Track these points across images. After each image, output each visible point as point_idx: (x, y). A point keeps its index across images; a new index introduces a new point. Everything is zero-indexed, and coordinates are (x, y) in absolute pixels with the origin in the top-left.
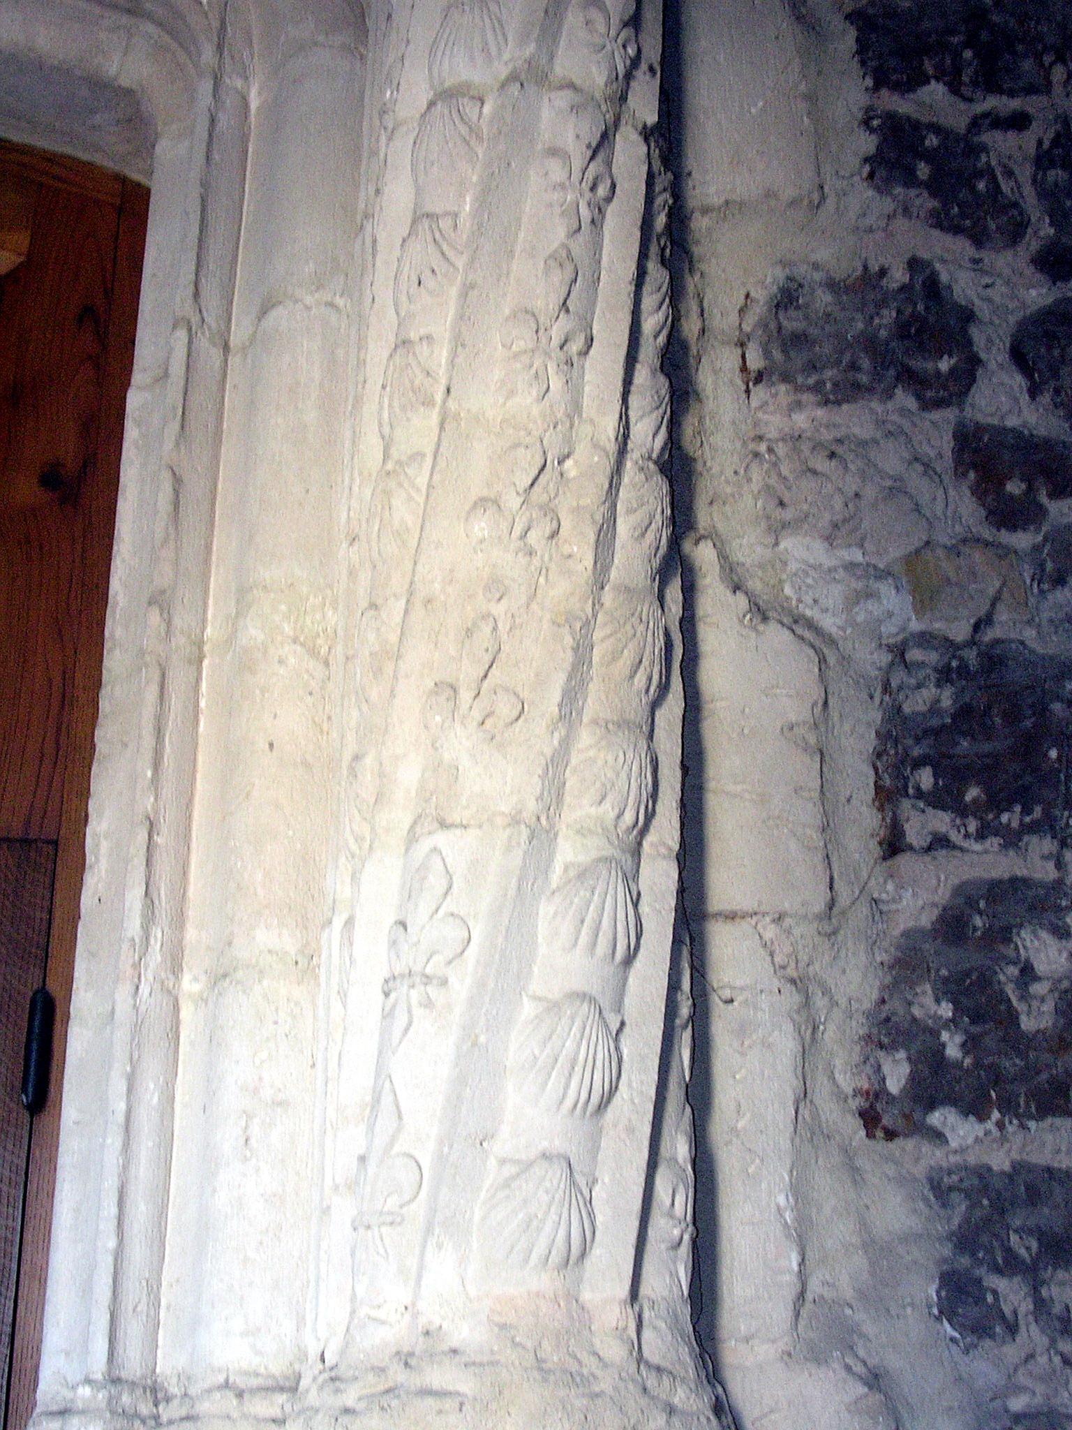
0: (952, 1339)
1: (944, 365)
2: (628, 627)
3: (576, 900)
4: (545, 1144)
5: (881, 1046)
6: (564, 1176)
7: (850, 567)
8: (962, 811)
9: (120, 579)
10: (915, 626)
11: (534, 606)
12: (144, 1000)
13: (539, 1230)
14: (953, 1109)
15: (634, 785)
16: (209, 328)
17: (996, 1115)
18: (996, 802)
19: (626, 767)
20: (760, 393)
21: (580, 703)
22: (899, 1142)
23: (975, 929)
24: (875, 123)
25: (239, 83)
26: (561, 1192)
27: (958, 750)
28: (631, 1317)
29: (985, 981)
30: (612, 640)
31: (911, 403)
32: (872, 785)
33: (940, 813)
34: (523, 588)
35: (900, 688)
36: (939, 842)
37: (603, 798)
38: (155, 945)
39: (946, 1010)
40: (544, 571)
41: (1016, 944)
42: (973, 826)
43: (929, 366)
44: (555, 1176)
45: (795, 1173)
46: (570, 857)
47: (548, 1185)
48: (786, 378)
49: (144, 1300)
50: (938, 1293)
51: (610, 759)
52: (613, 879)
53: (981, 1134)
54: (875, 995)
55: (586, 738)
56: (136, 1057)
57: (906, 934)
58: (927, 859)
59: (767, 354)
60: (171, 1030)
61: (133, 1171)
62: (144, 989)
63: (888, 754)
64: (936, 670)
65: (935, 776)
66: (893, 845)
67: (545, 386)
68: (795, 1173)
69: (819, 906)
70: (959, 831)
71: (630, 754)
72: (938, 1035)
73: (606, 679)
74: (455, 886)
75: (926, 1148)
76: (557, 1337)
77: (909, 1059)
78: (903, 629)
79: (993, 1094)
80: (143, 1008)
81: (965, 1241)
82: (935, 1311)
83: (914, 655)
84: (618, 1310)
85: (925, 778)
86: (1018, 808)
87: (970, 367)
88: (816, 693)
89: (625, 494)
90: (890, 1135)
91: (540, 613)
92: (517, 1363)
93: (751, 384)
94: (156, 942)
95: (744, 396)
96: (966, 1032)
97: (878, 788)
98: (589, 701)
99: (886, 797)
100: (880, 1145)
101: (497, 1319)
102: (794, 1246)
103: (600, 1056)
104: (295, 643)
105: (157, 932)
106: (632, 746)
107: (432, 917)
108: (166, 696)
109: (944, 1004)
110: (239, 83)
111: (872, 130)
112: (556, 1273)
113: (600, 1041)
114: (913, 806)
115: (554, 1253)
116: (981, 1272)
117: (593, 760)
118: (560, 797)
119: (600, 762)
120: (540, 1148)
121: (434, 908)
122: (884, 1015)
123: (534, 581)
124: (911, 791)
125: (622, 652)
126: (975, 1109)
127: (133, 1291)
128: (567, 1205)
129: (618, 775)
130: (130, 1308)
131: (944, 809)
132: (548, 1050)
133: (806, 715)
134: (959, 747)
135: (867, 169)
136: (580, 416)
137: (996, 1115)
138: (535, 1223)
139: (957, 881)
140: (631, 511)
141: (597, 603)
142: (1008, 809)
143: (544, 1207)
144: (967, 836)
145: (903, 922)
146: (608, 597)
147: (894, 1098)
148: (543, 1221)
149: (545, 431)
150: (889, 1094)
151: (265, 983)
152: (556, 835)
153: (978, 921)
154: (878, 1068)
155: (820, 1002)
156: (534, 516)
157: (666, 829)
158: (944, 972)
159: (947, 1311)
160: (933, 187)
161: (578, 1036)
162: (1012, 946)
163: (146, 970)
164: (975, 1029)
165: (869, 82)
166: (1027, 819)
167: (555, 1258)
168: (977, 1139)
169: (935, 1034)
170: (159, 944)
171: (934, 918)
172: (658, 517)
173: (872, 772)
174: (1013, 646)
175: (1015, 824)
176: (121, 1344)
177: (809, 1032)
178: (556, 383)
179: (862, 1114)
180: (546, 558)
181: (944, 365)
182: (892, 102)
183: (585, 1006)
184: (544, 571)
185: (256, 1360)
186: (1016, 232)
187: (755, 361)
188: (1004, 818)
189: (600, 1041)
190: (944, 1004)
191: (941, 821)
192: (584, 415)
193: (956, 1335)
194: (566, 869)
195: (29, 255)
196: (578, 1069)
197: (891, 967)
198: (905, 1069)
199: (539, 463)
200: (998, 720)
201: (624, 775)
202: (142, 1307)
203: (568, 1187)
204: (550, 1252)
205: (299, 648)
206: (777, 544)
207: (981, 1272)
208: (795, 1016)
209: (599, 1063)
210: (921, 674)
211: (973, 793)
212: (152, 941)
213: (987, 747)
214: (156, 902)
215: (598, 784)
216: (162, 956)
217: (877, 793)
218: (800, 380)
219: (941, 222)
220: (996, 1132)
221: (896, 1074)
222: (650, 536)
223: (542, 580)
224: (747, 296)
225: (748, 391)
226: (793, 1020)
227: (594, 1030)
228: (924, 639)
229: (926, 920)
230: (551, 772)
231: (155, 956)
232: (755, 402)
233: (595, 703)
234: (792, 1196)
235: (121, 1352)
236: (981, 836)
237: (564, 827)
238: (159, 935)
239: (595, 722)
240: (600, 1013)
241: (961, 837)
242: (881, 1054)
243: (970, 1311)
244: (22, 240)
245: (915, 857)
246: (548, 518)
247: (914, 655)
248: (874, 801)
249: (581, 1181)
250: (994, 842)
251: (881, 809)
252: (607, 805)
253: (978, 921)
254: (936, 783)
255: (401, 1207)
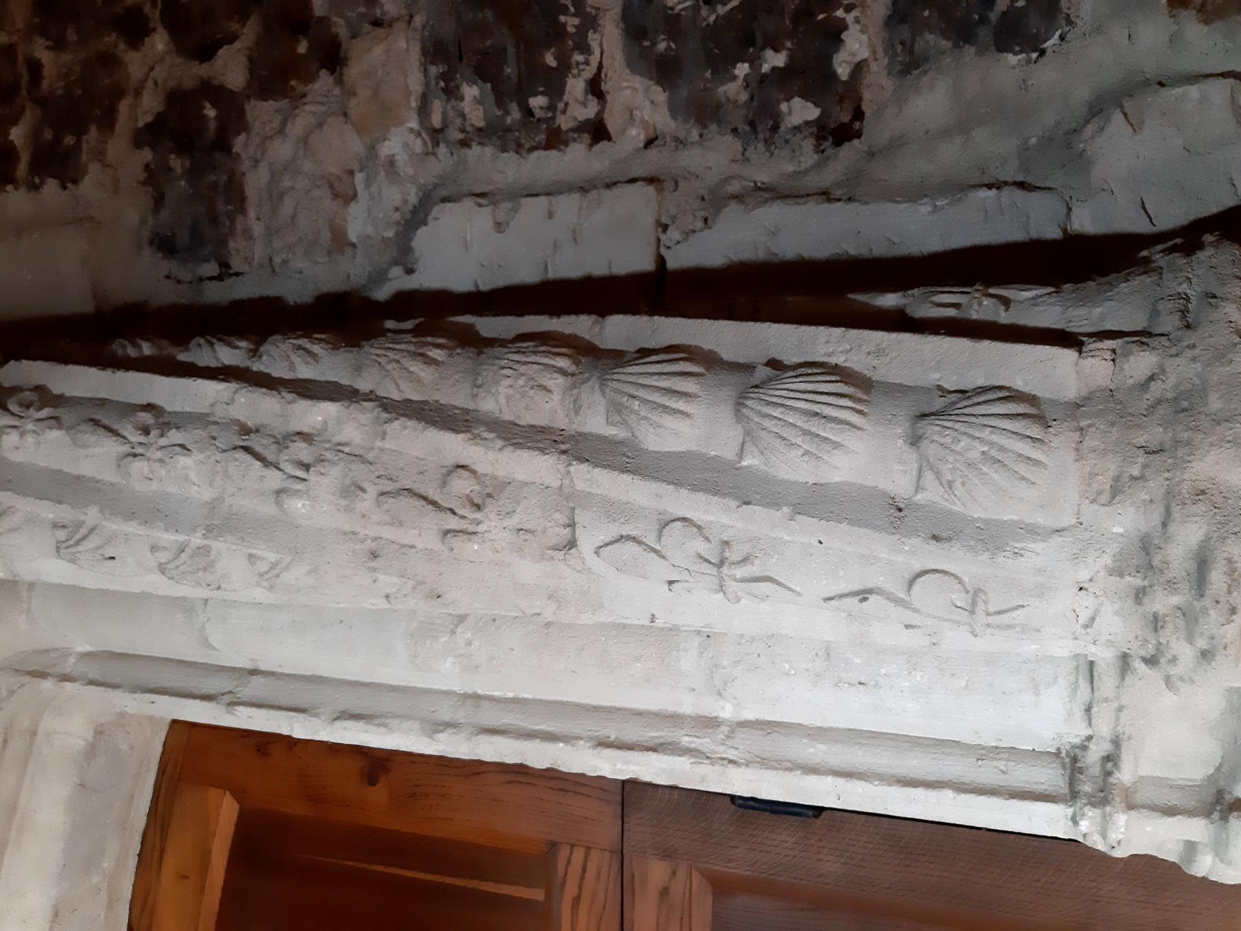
0: (1062, 38)
1: (211, 112)
2: (389, 367)
3: (642, 413)
4: (900, 442)
5: (775, 128)
6: (937, 422)
7: (368, 184)
8: (565, 67)
9: (426, 747)
10: (414, 124)
11: (370, 457)
12: (742, 755)
13: (1002, 449)
14: (835, 56)
15: (532, 358)
16: (237, 687)
17: (840, 13)
18: (559, 33)
19: (514, 367)
20: (236, 264)
21: (457, 411)
22: (865, 107)
23: (668, 48)
24: (37, 180)
25: (72, 660)
26: (957, 426)
27: (514, 76)
28: (1099, 345)
29: (713, 33)
30: (401, 382)
31: (241, 138)
32: (547, 152)
33: (568, 88)
34: (354, 468)
35: (462, 130)
36: (595, 88)
37: (545, 388)
38: (695, 743)
39: (742, 69)
40: (340, 448)
41: (681, 10)
42: (579, 58)
43: (212, 125)
44: (931, 429)
45: (898, 199)
46: (601, 419)
47: (948, 440)
48: (223, 242)
49: (995, 763)
50: (1015, 54)
51: (507, 382)
52: (622, 377)
53: (858, 27)
54: (729, 138)
55: (488, 405)
56: (788, 764)
57: (674, 114)
58: (608, 97)
59: (205, 260)
60: (764, 730)
61: (881, 770)
62: (732, 754)
63: (518, 137)
64: (449, 100)
65: (535, 95)
66: (597, 131)
67: (178, 449)
68: (898, 199)
69: (651, 190)
70: (584, 70)
71: (504, 363)
72: (765, 75)
73: (438, 387)
74: (633, 533)
75: (868, 80)
76: (1129, 428)
77: (788, 100)
78: (419, 135)
79: (821, 17)
80: (747, 756)
81: (962, 33)
82: (1034, 55)
83: (436, 120)
84: (1089, 359)
85: (538, 102)
86: (562, 18)
87: (212, 91)
88: (468, 203)
89: (278, 370)
90: (859, 114)
91: (376, 451)
92: (1167, 475)
93: (231, 272)
94: (694, 742)
95: (240, 277)
96: (763, 48)
97: (548, 146)
98: (456, 403)
99: (556, 140)
100: (868, 125)
101: (1105, 498)
102: (971, 195)
103: (803, 386)
104: (455, 633)
105: (686, 741)
106: (497, 362)
107: (663, 557)
108: (503, 728)
109: (737, 72)
110: (72, 660)
111: (42, 183)
112: (1051, 429)
113: (787, 386)
114: (564, 112)
115: (1028, 433)
116: (994, 16)
117: (508, 398)
118: (543, 430)
119: (511, 392)
120: (905, 448)
121: (653, 555)
122: (747, 128)
123: (347, 457)
124: (550, 115)
125: (412, 372)
126: (834, 34)
127: (988, 774)
128: (972, 419)
129: (522, 375)
130: (1003, 776)
131: (564, 85)
132: (799, 440)
133: (486, 211)
134: (512, 75)
135: (69, 185)
136: (208, 415)
137: (840, 13)
138: (994, 453)
139: (627, 71)
140: (292, 367)
141: (369, 397)
142: (564, 25)
143: (976, 443)
144: (587, 63)
145: (663, 120)
146: (364, 385)
147: (822, 112)
148: (991, 444)
149: (217, 448)
150: (819, 117)
151: (725, 663)
152: (580, 434)
153: (662, 46)
154: (797, 129)
155: (735, 187)
156: (286, 458)
157: (579, 325)
158: (708, 74)
159: (1034, 45)
160: (80, 132)
161: (781, 409)
162: (683, 13)
163: (716, 752)
164: (760, 40)
165: (10, 188)
166: (572, 9)
167: (1035, 430)
168: (862, 31)
169: (763, 79)
170: (695, 740)
171: (660, 89)
172: (301, 342)
173: (536, 154)
174: (427, 34)
175: (576, 21)
176: (1036, 787)
177: (761, 193)
178: (174, 436)
179: (838, 143)
180: (327, 446)
181: (211, 112)
182: (22, 169)
183: (749, 403)
184: (340, 448)
185: (1062, 682)
186: (109, 61)
187: (211, 269)
188: (571, 30)
189: (787, 386)
190: (737, 72)
191: (576, 86)
192: (209, 411)
193: (1058, 33)
194: (612, 424)
195: (225, 789)
196: (816, 408)
197: (704, 126)
198: (797, 101)
199: (241, 455)
200: (488, 43)
201: (523, 369)
202: (1002, 765)
203: (953, 418)
204: (1028, 437)
205: (459, 630)
206: (354, 245)
207: (994, 16)
208: (750, 207)
209: (810, 387)
210: (451, 113)
211: (550, 60)
212: (693, 746)
213: (511, 50)
214: (662, 740)
215: (531, 393)
216: (705, 737)
217: (554, 148)
218: (227, 231)
219: (108, 122)
220: (854, 13)
221: (800, 111)
222: (316, 348)
223: (347, 450)
224: (168, 277)
225: (237, 274)
226: (753, 209)
227: (774, 394)
228: (424, 110)
229: (660, 95)
230: (521, 441)
231: (703, 742)
232: (245, 268)
233: (456, 395)
234: (922, 199)
235: (1043, 787)
236: (585, 49)
237: (574, 426)
238: (687, 739)
239: (475, 396)
240: (756, 387)
241: (587, 68)
242: (783, 128)
243: (1034, 23)
244: (213, 792)
245: (607, 111)
246: (291, 444)
247: (436, 120)
248: (560, 150)
249: (939, 404)
250: (593, 38)
251: (566, 144)
252: (551, 384)
253: (662, 46)
254: (543, 93)
255: (967, 592)
